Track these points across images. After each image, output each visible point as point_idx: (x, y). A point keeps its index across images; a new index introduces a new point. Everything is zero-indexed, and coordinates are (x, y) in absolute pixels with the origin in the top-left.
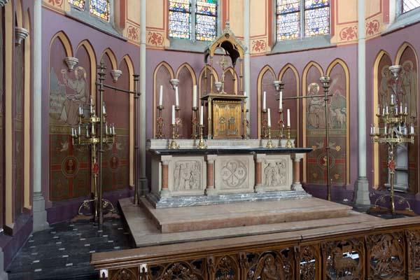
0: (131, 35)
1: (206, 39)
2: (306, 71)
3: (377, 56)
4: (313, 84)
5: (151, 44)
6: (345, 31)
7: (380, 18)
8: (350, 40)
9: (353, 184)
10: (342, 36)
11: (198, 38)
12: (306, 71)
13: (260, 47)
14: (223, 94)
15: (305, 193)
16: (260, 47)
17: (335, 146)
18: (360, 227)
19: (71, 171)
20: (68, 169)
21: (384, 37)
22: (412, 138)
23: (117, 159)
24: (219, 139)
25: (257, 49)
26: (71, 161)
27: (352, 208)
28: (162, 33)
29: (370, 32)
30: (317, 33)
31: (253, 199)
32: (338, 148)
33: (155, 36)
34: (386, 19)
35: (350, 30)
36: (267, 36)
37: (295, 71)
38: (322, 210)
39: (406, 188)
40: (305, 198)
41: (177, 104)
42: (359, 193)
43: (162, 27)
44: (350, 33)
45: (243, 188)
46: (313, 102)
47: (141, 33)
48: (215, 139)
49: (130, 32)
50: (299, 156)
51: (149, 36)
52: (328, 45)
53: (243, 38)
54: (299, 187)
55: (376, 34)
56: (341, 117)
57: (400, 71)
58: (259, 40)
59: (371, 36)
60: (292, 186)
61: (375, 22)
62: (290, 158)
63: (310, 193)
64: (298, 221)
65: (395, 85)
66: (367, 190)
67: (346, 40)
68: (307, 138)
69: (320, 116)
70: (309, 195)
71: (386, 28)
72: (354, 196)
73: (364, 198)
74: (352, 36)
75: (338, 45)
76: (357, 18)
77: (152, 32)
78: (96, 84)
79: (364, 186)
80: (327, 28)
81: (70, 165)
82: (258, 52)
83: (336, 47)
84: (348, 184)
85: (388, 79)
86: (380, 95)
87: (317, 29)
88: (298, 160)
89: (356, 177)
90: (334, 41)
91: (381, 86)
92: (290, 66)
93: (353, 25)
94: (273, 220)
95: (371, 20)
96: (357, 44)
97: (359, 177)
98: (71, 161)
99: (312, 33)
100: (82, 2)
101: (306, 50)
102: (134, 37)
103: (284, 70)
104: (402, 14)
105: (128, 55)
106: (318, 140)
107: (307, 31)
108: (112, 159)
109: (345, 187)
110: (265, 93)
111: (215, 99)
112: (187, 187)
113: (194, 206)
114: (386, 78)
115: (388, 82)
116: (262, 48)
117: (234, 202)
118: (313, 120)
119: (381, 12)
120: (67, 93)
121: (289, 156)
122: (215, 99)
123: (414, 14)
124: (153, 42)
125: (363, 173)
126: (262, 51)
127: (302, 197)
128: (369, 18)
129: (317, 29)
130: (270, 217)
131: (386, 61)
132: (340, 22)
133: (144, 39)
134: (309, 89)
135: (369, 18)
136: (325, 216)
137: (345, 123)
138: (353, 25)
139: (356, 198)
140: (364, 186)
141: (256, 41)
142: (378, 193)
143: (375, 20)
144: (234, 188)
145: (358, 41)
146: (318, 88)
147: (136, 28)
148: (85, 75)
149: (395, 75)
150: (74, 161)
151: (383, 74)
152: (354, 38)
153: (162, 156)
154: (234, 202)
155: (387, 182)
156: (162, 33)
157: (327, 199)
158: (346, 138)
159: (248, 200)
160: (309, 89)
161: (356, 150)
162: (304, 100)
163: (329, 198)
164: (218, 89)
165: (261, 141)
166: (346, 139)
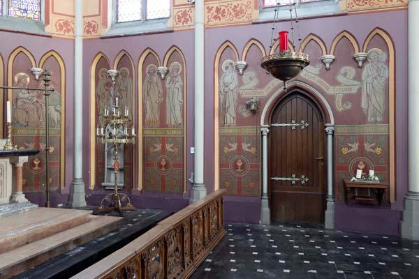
3: (94, 59)
4: (22, 74)
5: (214, 22)
6: (61, 22)
7: (99, 20)
8: (67, 34)
9: (67, 186)
10: (58, 28)
13: (91, 30)
15: (30, 204)
17: (374, 148)
18: (97, 232)
21: (102, 40)
22: (134, 139)
27: (92, 212)
29: (88, 32)
30: (25, 15)
32: (378, 151)
34: (105, 24)
35: (66, 23)
36: (101, 17)
38: (67, 220)
39: (122, 185)
40: (31, 210)
42: (75, 196)
43: (98, 13)
44: (66, 26)
46: (21, 95)
50: (23, 160)
52: (42, 33)
53: (74, 17)
54: (21, 197)
55: (93, 35)
56: (55, 115)
57: (117, 76)
58: (90, 21)
59: (89, 36)
60: (11, 198)
61: (93, 23)
62: (8, 163)
63: (35, 203)
64: (43, 238)
65: (112, 88)
66: (83, 190)
67: (62, 33)
68: (143, 138)
69: (31, 113)
70: (36, 206)
71: (106, 32)
72: (69, 200)
73: (80, 198)
74: (68, 31)
75: (53, 35)
76: (74, 11)
79: (80, 189)
80: (37, 13)
83: (50, 37)
84: (62, 188)
85: (104, 82)
86: (97, 96)
87: (26, 11)
88: (20, 165)
89: (71, 179)
90: (50, 29)
91: (99, 86)
93: (70, 19)
94: (14, 244)
95: (90, 19)
96: (74, 40)
97: (74, 179)
99: (19, 13)
101: (13, 32)
102: (187, 21)
104: (117, 23)
105: (254, 39)
106: (27, 139)
107: (12, 9)
109: (59, 191)
114: (102, 82)
115: (105, 84)
116: (94, 30)
118: (22, 118)
119: (99, 15)
121: (7, 160)
123: (130, 26)
125: (79, 174)
127: (27, 208)
128: (87, 17)
129: (26, 11)
130: (8, 242)
131: (103, 63)
132: (55, 11)
134: (16, 79)
135: (87, 17)
136: (67, 226)
137: (59, 122)
138: (70, 19)
139: (72, 201)
140: (80, 189)
142: (93, 193)
143: (94, 21)
145: (75, 37)
146: (28, 80)
149: (113, 79)
150: (242, 161)
151: (100, 76)
152: (71, 33)
155: (104, 182)
157: (46, 206)
158: (183, 138)
160: (16, 79)
161: (71, 151)
162: (10, 91)
163: (49, 205)
166: (60, 140)
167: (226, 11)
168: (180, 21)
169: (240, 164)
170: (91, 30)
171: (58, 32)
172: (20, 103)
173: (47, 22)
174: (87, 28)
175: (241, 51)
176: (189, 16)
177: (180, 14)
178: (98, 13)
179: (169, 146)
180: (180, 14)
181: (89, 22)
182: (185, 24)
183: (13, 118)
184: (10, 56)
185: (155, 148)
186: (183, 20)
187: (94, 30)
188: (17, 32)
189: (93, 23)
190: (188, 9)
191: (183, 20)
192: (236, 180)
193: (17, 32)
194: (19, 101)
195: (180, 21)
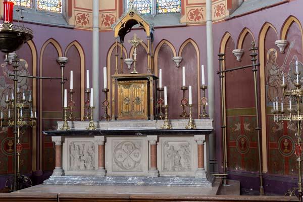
0: (80, 22)
1: (169, 11)
2: (44, 47)
5: (104, 26)
6: (79, 15)
11: (160, 11)
12: (44, 47)
14: (134, 73)
16: (220, 12)
19: (243, 148)
20: (241, 147)
23: (245, 140)
24: (123, 120)
25: (218, 14)
26: (243, 140)
28: (114, 14)
31: (139, 183)
33: (108, 18)
36: (118, 11)
37: (67, 50)
41: (71, 87)
43: (114, 8)
45: (137, 171)
47: (93, 18)
48: (120, 120)
49: (79, 18)
51: (102, 19)
53: (92, 10)
58: (108, 14)
61: (112, 17)
77: (105, 14)
78: (259, 65)
81: (243, 143)
82: (219, 18)
83: (73, 29)
90: (72, 22)
92: (76, 43)
98: (243, 140)
100: (29, 2)
102: (85, 23)
103: (68, 47)
108: (240, 140)
110: (161, 70)
111: (119, 80)
112: (82, 167)
113: (78, 185)
116: (222, 13)
117: (118, 184)
120: (7, 83)
122: (119, 80)
124: (106, 24)
126: (222, 16)
133: (96, 23)
141: (105, 14)
144: (127, 170)
146: (276, 54)
147: (86, 13)
148: (26, 66)
150: (288, 140)
153: (53, 137)
154: (118, 184)
156: (114, 14)
159: (133, 184)
164: (129, 67)
165: (193, 121)
167: (114, 19)
168: (192, 18)
169: (286, 144)
170: (109, 22)
171: (77, 25)
172: (271, 80)
173: (70, 15)
174: (217, 12)
175: (129, 51)
176: (87, 20)
177: (192, 11)
178: (114, 8)
179: (247, 126)
180: (192, 11)
181: (107, 15)
182: (197, 21)
183: (10, 116)
184: (259, 35)
185: (236, 127)
186: (195, 17)
187: (222, 13)
188: (262, 9)
189: (112, 17)
190: (199, 8)
191: (195, 17)
192: (7, 159)
193: (262, 9)
194: (271, 79)
195: (192, 18)
